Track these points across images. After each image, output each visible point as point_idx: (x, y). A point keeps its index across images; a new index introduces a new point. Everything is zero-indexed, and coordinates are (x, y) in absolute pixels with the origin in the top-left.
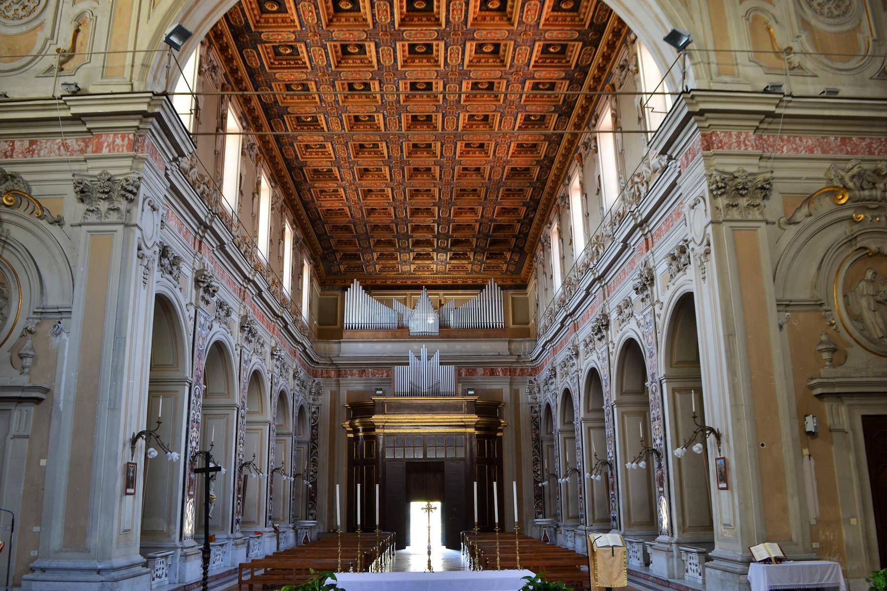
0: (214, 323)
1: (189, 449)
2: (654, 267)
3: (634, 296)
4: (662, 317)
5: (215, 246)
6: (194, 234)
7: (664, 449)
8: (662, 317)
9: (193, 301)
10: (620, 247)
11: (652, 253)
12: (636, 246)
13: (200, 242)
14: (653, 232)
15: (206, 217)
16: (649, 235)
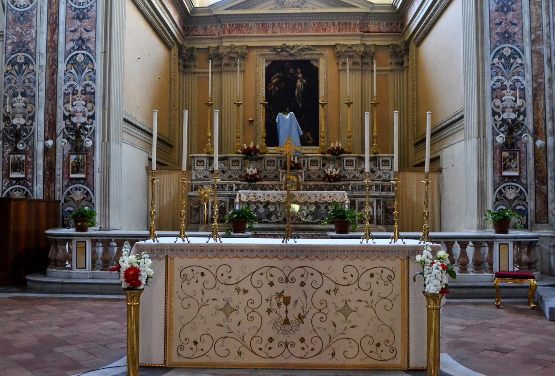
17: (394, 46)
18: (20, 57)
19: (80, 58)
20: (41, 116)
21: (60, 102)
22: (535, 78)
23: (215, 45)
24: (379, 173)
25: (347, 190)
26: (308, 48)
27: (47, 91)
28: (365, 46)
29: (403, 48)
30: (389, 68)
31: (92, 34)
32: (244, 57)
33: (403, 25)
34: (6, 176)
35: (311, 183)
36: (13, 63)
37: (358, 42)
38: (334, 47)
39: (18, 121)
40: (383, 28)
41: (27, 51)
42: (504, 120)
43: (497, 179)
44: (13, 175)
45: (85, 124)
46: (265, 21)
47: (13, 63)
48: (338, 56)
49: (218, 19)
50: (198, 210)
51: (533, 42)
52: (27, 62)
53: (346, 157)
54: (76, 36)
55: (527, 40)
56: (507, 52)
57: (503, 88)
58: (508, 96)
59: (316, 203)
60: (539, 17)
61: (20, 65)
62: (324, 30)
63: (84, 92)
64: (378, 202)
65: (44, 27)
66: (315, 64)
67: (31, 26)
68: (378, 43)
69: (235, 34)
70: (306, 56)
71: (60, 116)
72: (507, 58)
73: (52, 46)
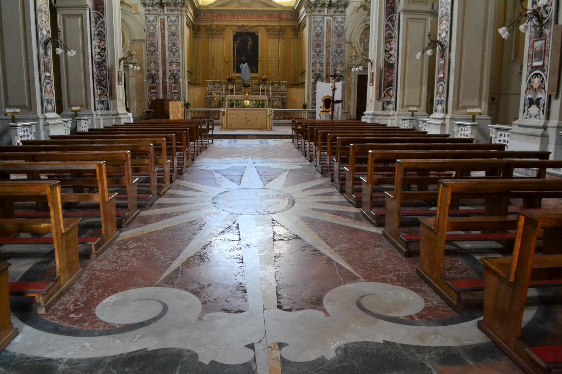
1: (40, 36)
17: (294, 26)
19: (174, 50)
20: (160, 70)
21: (167, 65)
22: (327, 59)
23: (210, 24)
24: (280, 88)
26: (254, 27)
27: (162, 61)
28: (280, 26)
29: (297, 28)
30: (292, 36)
31: (178, 41)
32: (223, 30)
33: (298, 15)
34: (150, 91)
35: (254, 92)
36: (149, 51)
37: (277, 24)
38: (266, 26)
39: (153, 72)
40: (289, 17)
41: (155, 47)
42: (316, 74)
43: (530, 69)
44: (152, 91)
45: (176, 73)
46: (234, 14)
47: (149, 51)
48: (268, 30)
49: (211, 11)
50: (210, 103)
51: (327, 47)
52: (155, 51)
53: (268, 82)
54: (172, 42)
55: (325, 46)
56: (318, 50)
57: (316, 63)
58: (318, 66)
59: (256, 100)
60: (330, 38)
61: (152, 52)
62: (261, 18)
63: (176, 62)
65: (160, 38)
67: (155, 38)
68: (287, 24)
69: (219, 19)
70: (252, 30)
71: (167, 70)
72: (318, 53)
73: (163, 45)
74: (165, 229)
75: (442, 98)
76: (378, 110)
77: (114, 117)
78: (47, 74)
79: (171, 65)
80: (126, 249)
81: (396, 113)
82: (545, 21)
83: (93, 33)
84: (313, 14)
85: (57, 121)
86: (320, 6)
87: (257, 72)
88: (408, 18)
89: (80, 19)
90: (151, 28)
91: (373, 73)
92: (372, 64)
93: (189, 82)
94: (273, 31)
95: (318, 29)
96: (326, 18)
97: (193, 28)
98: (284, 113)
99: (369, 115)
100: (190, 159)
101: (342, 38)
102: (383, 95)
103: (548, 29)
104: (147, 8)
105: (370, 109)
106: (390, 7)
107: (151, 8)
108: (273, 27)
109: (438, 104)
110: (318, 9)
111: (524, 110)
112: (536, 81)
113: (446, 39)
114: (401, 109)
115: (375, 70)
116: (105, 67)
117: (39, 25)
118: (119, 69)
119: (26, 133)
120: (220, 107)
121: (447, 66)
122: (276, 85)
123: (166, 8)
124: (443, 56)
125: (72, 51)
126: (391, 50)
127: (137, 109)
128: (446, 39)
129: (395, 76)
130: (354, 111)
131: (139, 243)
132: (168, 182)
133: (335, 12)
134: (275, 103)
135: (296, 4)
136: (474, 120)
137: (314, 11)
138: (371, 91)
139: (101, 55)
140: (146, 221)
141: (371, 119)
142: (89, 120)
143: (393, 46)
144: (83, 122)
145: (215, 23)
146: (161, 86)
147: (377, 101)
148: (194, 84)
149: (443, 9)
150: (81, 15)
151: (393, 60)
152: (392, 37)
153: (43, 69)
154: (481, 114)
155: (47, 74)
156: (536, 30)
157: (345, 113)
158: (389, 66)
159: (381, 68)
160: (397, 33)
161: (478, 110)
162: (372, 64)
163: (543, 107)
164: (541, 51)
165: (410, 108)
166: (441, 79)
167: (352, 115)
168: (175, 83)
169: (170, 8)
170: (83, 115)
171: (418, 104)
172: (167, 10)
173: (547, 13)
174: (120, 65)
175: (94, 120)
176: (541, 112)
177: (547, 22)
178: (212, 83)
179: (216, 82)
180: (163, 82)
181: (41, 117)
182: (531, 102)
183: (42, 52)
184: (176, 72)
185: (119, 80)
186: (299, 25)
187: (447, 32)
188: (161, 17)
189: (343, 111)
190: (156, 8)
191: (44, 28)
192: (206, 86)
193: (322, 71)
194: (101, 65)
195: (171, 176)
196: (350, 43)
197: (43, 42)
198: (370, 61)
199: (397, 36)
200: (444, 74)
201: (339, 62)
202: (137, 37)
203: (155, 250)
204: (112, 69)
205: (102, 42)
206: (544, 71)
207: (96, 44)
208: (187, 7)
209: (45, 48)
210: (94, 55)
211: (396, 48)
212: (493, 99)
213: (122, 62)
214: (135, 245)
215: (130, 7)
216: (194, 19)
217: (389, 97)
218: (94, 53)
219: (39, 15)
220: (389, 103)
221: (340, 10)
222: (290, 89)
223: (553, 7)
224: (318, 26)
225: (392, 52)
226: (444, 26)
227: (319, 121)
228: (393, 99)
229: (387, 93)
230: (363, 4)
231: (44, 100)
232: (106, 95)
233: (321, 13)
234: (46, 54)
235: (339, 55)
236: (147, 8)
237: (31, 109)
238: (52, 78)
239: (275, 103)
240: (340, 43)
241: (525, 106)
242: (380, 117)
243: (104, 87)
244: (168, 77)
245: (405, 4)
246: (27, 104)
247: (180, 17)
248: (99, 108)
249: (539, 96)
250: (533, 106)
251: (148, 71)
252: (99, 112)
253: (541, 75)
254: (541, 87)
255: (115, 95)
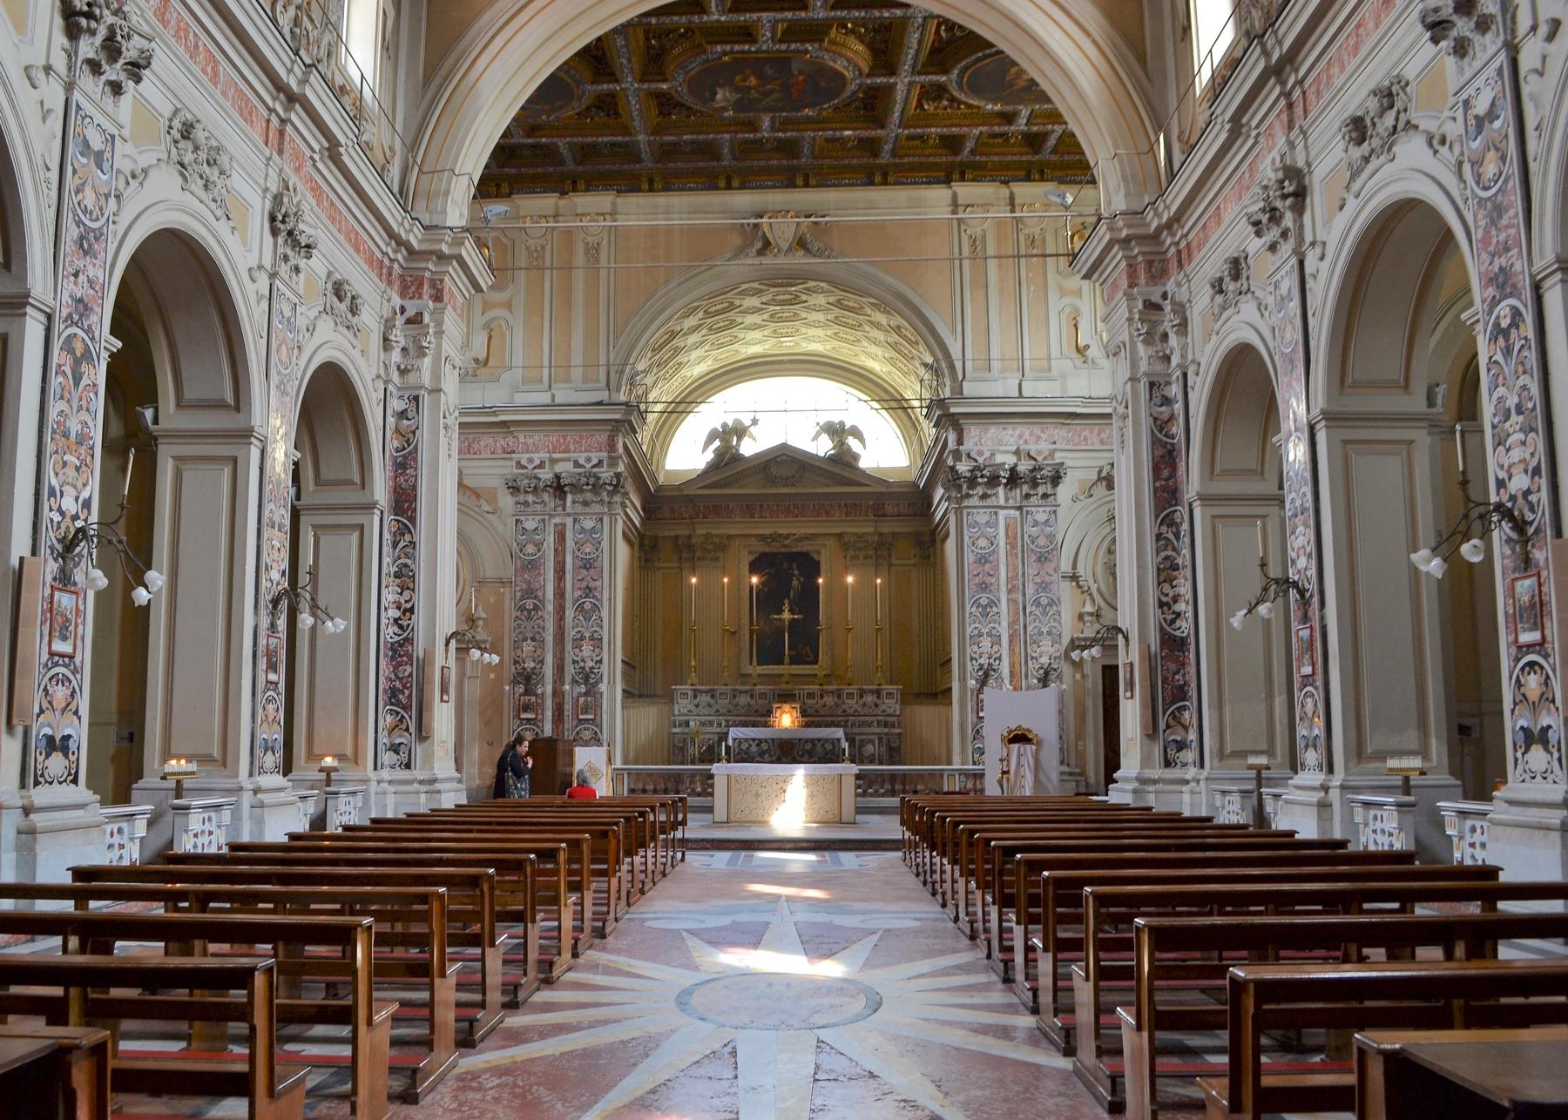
0: (321, 324)
1: (264, 584)
2: (1309, 165)
3: (1255, 245)
4: (1322, 277)
5: (317, 147)
6: (265, 113)
7: (1314, 579)
8: (1322, 277)
9: (267, 263)
10: (1224, 136)
11: (1303, 132)
12: (1262, 129)
13: (282, 133)
14: (1190, 237)
15: (290, 71)
16: (1183, 244)
18: (529, 604)
19: (588, 606)
20: (549, 659)
21: (569, 646)
22: (1011, 625)
23: (686, 532)
24: (883, 707)
25: (845, 726)
28: (880, 534)
31: (598, 583)
33: (930, 505)
36: (522, 609)
37: (871, 530)
38: (840, 536)
39: (530, 664)
43: (1513, 650)
47: (522, 609)
49: (690, 499)
50: (682, 749)
51: (1009, 591)
52: (536, 608)
55: (1003, 589)
57: (981, 635)
60: (1016, 568)
61: (529, 611)
63: (592, 638)
64: (880, 739)
66: (816, 557)
71: (568, 660)
73: (560, 594)
74: (562, 1054)
75: (1316, 732)
76: (1153, 767)
77: (424, 788)
78: (272, 677)
79: (580, 647)
80: (478, 1089)
81: (1205, 773)
82: (1531, 530)
83: (385, 571)
84: (966, 503)
85: (282, 797)
86: (986, 484)
87: (816, 662)
88: (1214, 517)
89: (355, 536)
90: (530, 549)
91: (1132, 664)
92: (1127, 639)
93: (624, 691)
94: (860, 549)
95: (982, 542)
96: (1002, 513)
97: (641, 545)
98: (893, 777)
99: (1127, 780)
100: (623, 902)
101: (1049, 567)
102: (1162, 726)
103: (1541, 548)
104: (521, 498)
105: (1130, 765)
106: (1164, 488)
107: (530, 498)
108: (860, 536)
109: (1307, 747)
110: (980, 490)
111: (1516, 760)
112: (1533, 682)
113: (1309, 573)
114: (1216, 761)
115: (1135, 655)
116: (410, 658)
117: (265, 558)
118: (443, 659)
119: (207, 827)
120: (711, 762)
121: (1318, 645)
122: (869, 699)
123: (569, 498)
124: (1305, 618)
125: (337, 620)
126: (1175, 601)
127: (481, 764)
128: (1309, 573)
129: (1193, 670)
130: (1097, 768)
131: (508, 1079)
132: (567, 955)
133: (1028, 496)
134: (869, 749)
135: (921, 475)
136: (1407, 788)
137: (968, 496)
138: (1131, 713)
139: (401, 627)
140: (516, 1037)
141: (1135, 791)
142: (360, 796)
143: (1182, 590)
144: (343, 799)
145: (700, 532)
146: (549, 702)
147: (1147, 741)
148: (640, 696)
149: (1293, 495)
150: (362, 527)
151: (1185, 626)
152: (1176, 568)
153: (262, 664)
154: (1423, 773)
155: (272, 677)
156: (1513, 551)
157: (1071, 774)
158: (1174, 645)
159: (1153, 649)
160: (1188, 557)
161: (1416, 762)
162: (1127, 639)
163: (1559, 750)
164: (1532, 606)
165: (1252, 760)
166: (1307, 680)
167: (1092, 781)
168: (585, 694)
169: (580, 498)
170: (342, 782)
171: (1265, 747)
172: (574, 502)
173: (1532, 510)
174: (447, 651)
175: (375, 795)
176: (1556, 763)
177: (1537, 531)
178: (691, 694)
179: (701, 692)
180: (555, 692)
181: (248, 784)
182: (1531, 738)
183: (265, 621)
184: (591, 664)
185: (444, 690)
186: (933, 532)
187: (1310, 556)
188: (557, 520)
189: (1066, 769)
190: (546, 497)
191: (275, 565)
192: (672, 701)
193: (999, 658)
194: (400, 651)
195: (576, 940)
196: (1074, 578)
197: (269, 598)
198: (1120, 630)
199: (1188, 563)
200: (1313, 665)
201: (1045, 630)
202: (490, 572)
203: (543, 1091)
204: (424, 665)
205: (407, 594)
206: (1546, 657)
207: (391, 598)
208: (626, 494)
209: (273, 614)
210: (383, 626)
211: (1189, 596)
212: (1464, 730)
213: (453, 643)
214: (497, 1081)
215: (478, 496)
216: (644, 521)
217: (1180, 730)
218: (384, 621)
219: (265, 535)
220: (1181, 746)
221: (1041, 490)
222: (909, 709)
223: (1544, 495)
224: (983, 535)
225: (1180, 607)
226: (1301, 541)
227: (995, 800)
228: (1192, 736)
229: (1175, 717)
230: (1104, 474)
231: (257, 743)
232: (407, 730)
233: (989, 502)
234: (273, 626)
235: (1045, 613)
236: (521, 498)
237: (225, 765)
238: (282, 687)
239: (869, 749)
240: (1047, 579)
241: (1516, 750)
242: (1160, 786)
243: (404, 708)
244: (568, 679)
245: (1202, 480)
246: (216, 753)
247: (606, 519)
248: (386, 763)
249: (1545, 721)
250: (1534, 747)
251: (516, 662)
252: (385, 774)
253: (1542, 668)
254: (1547, 699)
255: (430, 729)
